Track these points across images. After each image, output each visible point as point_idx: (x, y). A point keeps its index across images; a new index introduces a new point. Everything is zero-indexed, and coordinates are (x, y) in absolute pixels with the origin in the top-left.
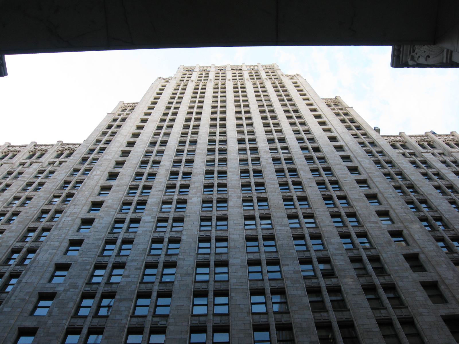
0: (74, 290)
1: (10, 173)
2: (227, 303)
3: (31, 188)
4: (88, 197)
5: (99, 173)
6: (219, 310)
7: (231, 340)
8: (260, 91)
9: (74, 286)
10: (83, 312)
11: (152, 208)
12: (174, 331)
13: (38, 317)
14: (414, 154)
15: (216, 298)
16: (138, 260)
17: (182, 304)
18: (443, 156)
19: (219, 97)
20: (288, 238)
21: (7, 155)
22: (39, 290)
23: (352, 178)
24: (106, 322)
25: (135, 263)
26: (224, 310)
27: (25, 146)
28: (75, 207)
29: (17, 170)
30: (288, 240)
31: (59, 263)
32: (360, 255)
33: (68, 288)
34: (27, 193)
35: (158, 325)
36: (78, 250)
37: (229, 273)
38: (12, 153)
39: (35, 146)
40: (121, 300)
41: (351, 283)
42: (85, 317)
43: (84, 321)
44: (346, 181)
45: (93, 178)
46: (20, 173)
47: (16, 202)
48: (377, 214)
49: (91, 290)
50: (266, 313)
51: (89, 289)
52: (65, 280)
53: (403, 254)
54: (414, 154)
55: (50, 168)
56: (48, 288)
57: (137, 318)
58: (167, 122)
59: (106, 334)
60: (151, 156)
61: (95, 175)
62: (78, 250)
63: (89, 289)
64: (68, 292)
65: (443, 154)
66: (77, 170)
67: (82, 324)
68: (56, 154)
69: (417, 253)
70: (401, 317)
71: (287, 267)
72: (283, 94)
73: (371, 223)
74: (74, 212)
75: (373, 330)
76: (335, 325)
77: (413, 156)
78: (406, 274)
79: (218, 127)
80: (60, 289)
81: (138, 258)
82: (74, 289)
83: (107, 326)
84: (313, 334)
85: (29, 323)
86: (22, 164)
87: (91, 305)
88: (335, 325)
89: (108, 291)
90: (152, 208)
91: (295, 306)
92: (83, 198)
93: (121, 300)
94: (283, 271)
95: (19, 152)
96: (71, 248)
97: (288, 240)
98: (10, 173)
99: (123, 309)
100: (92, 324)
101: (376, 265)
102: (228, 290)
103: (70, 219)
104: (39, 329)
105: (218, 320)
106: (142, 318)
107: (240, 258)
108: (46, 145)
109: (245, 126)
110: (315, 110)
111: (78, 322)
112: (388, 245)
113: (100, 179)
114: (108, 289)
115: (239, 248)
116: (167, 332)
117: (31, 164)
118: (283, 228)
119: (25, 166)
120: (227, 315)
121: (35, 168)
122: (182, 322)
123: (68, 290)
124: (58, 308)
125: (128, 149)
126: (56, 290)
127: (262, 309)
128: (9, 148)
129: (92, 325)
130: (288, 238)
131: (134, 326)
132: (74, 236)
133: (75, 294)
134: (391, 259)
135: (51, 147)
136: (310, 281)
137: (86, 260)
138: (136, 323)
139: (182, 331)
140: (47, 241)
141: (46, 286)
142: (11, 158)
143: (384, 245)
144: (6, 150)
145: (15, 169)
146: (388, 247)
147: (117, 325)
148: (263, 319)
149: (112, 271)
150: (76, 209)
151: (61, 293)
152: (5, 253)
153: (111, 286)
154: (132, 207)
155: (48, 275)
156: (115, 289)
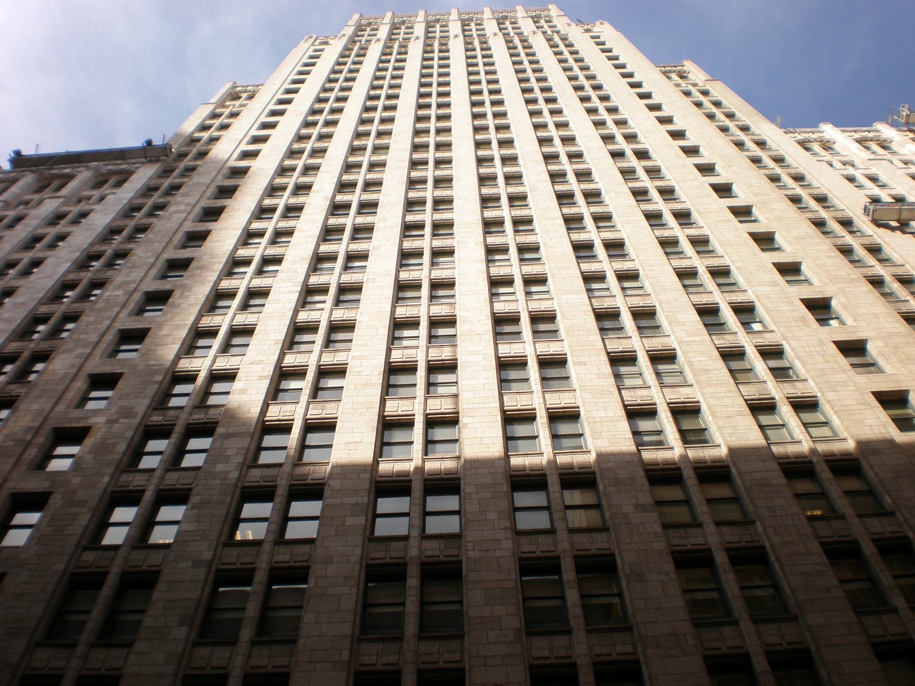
0: (127, 420)
2: (457, 508)
4: (159, 252)
5: (182, 207)
6: (434, 525)
7: (462, 507)
8: (551, 126)
9: (127, 413)
10: (147, 462)
11: (295, 267)
12: (340, 490)
13: (120, 360)
15: (429, 498)
16: (265, 362)
17: (359, 440)
19: (434, 95)
20: (585, 314)
22: (53, 423)
23: (740, 230)
24: (194, 479)
25: (258, 368)
26: (451, 525)
28: (132, 270)
30: (585, 317)
31: (97, 372)
32: (772, 396)
33: (114, 417)
35: (306, 480)
36: (136, 350)
37: (463, 512)
40: (227, 436)
41: (723, 395)
42: (151, 471)
43: (147, 478)
44: (707, 210)
45: (170, 219)
48: (806, 306)
49: (165, 421)
50: (552, 531)
51: (160, 418)
52: (109, 404)
53: (834, 342)
56: (74, 419)
57: (261, 469)
58: (340, 81)
59: (194, 499)
60: (283, 195)
61: (176, 212)
62: (136, 350)
63: (160, 418)
64: (116, 425)
66: (117, 231)
67: (143, 483)
69: (864, 338)
70: (881, 536)
71: (583, 366)
72: (587, 84)
73: (762, 285)
74: (129, 279)
75: (774, 482)
76: (721, 558)
78: (840, 377)
79: (433, 119)
80: (100, 420)
81: (264, 358)
82: (126, 417)
83: (196, 485)
84: (642, 491)
85: (33, 484)
87: (163, 449)
88: (721, 558)
89: (201, 421)
90: (295, 267)
91: (602, 438)
92: (149, 254)
93: (227, 436)
94: (605, 507)
96: (94, 394)
97: (585, 317)
99: (231, 452)
100: (164, 484)
101: (852, 484)
102: (460, 562)
103: (120, 292)
104: (53, 496)
105: (433, 549)
106: (272, 469)
107: (482, 352)
109: (498, 162)
110: (638, 85)
111: (137, 481)
112: (801, 324)
113: (185, 220)
114: (199, 417)
115: (480, 334)
116: (327, 492)
118: (573, 297)
120: (458, 537)
122: (358, 474)
123: (115, 421)
124: (93, 455)
125: (229, 183)
126: (88, 422)
127: (541, 521)
129: (87, 669)
130: (585, 314)
131: (257, 484)
132: (128, 324)
133: (127, 428)
134: (808, 349)
136: (633, 394)
137: (154, 365)
138: (259, 478)
139: (358, 491)
140: (70, 337)
141: (69, 416)
143: (793, 324)
146: (803, 328)
147: (218, 482)
148: (542, 546)
149: (155, 510)
150: (133, 275)
151: (100, 428)
153: (207, 411)
154: (217, 343)
155: (73, 395)
156: (214, 417)
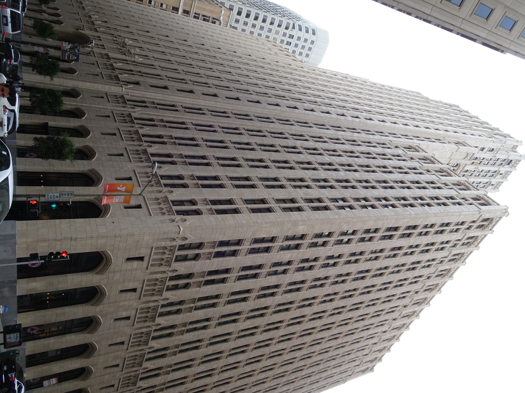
1: (414, 169)
3: (436, 201)
14: (468, 229)
18: (426, 278)
21: (479, 200)
27: (498, 205)
29: (459, 200)
34: (431, 202)
38: (465, 187)
39: (485, 195)
46: (439, 188)
47: (419, 200)
54: (468, 229)
55: (462, 201)
65: (454, 246)
68: (474, 196)
77: (468, 226)
86: (446, 185)
95: (470, 190)
98: (452, 198)
108: (493, 201)
117: (471, 204)
119: (466, 202)
121: (453, 193)
128: (485, 197)
135: (496, 204)
142: (461, 189)
144: (482, 196)
145: (458, 198)
152: (217, 107)
